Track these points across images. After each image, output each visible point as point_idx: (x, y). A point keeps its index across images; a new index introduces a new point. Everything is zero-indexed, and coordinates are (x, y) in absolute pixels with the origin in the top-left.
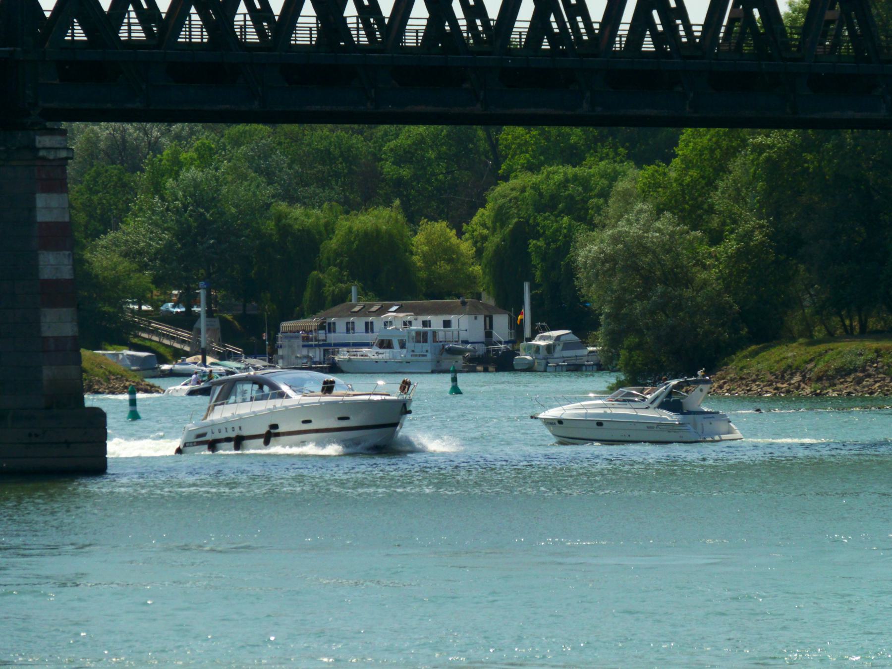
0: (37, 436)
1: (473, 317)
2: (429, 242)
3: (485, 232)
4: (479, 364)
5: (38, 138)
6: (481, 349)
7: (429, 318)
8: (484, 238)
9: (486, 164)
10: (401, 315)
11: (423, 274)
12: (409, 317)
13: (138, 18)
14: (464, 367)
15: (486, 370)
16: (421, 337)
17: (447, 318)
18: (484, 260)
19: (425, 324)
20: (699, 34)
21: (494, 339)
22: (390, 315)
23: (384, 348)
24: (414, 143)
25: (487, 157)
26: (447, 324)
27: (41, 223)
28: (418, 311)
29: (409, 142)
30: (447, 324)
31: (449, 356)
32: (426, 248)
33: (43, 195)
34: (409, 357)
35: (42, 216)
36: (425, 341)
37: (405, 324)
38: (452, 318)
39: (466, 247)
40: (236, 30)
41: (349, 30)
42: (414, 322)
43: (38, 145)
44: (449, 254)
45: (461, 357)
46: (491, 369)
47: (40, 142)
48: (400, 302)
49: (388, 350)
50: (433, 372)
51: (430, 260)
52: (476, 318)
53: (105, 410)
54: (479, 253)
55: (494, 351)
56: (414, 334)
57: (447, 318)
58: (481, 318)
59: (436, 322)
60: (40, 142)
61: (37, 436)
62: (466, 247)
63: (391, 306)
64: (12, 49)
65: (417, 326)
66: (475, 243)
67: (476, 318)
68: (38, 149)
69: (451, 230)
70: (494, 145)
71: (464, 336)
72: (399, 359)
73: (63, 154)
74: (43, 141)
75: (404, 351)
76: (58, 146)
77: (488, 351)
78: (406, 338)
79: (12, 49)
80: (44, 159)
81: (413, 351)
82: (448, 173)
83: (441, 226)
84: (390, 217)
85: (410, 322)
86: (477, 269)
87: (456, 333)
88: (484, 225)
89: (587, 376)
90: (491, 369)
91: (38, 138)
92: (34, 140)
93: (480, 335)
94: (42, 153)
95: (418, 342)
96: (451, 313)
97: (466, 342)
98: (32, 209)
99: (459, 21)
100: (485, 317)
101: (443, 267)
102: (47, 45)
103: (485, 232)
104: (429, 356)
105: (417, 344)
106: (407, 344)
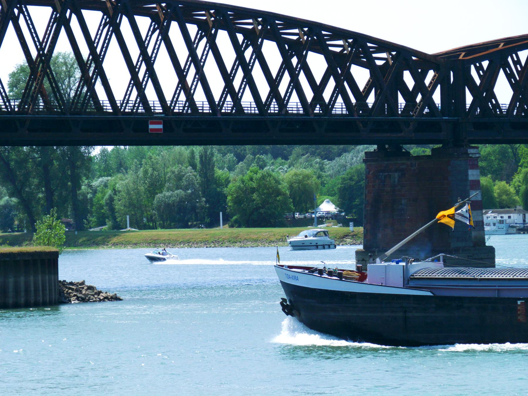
0: (471, 256)
1: (519, 214)
2: (499, 189)
3: (520, 184)
4: (522, 231)
5: (469, 150)
6: (522, 226)
7: (503, 215)
8: (519, 186)
9: (513, 161)
10: (493, 214)
11: (498, 200)
12: (495, 215)
13: (345, 105)
14: (516, 232)
15: (524, 233)
16: (501, 222)
17: (509, 215)
18: (520, 195)
19: (502, 217)
20: (42, 107)
21: (526, 222)
22: (488, 215)
23: (487, 226)
24: (487, 154)
25: (512, 158)
26: (509, 217)
27: (470, 180)
28: (499, 213)
29: (485, 154)
30: (509, 217)
31: (511, 228)
32: (499, 191)
33: (471, 170)
34: (497, 229)
35: (471, 178)
36: (503, 223)
37: (494, 217)
38: (511, 215)
39: (512, 190)
40: (43, 104)
41: (100, 103)
42: (497, 217)
43: (469, 152)
44: (506, 192)
45: (515, 229)
46: (526, 233)
47: (469, 151)
48: (492, 210)
49: (489, 227)
50: (506, 234)
51: (500, 195)
52: (520, 215)
53: (494, 246)
54: (517, 192)
55: (526, 226)
56: (498, 221)
57: (509, 215)
58: (521, 215)
59: (506, 216)
60: (469, 151)
61: (471, 256)
62: (512, 190)
63: (489, 211)
64: (458, 118)
65: (499, 218)
66: (515, 188)
67: (520, 215)
68: (469, 154)
69: (507, 184)
70: (515, 154)
71: (516, 221)
72: (493, 230)
73: (478, 155)
74: (470, 151)
75: (495, 227)
76: (476, 153)
77: (524, 227)
78: (496, 222)
79: (458, 118)
80: (471, 157)
81: (498, 227)
82: (499, 164)
83: (504, 183)
84: (487, 180)
85: (496, 217)
86: (517, 198)
87: (513, 221)
88: (520, 182)
89: (6, 252)
90: (526, 233)
91: (469, 150)
92: (467, 151)
93: (522, 222)
94: (470, 155)
95: (501, 224)
96: (511, 213)
97: (516, 223)
98: (467, 175)
99: (149, 102)
100: (523, 214)
101: (504, 197)
102: (469, 117)
103: (520, 184)
104: (505, 229)
105: (500, 225)
106: (496, 224)
